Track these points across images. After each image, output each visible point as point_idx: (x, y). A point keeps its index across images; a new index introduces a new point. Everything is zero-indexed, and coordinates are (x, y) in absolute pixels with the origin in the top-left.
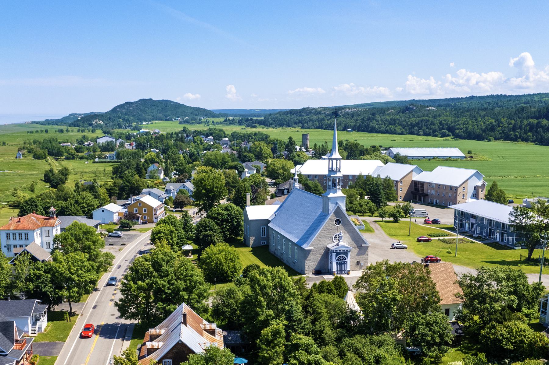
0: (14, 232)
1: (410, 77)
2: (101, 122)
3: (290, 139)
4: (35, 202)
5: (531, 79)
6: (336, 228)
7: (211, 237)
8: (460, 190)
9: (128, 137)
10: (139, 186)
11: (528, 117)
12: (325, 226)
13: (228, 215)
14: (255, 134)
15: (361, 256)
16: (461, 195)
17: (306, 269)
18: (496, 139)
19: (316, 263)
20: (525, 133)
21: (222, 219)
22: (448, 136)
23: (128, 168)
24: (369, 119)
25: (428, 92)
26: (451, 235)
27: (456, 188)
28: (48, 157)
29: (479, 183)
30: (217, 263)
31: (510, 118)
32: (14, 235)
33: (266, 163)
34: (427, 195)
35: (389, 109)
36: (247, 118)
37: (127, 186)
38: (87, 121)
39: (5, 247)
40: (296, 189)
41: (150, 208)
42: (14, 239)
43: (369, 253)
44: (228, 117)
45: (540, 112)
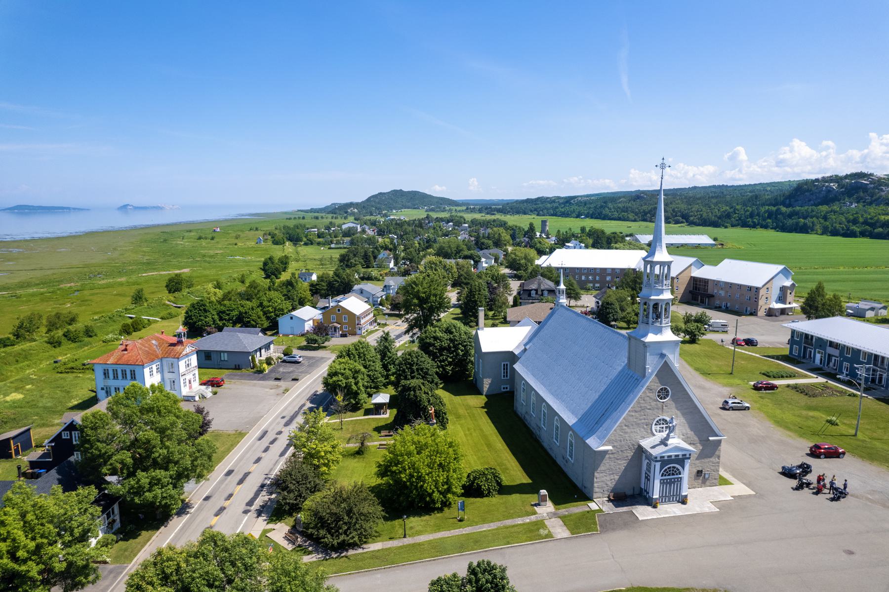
0: (115, 367)
1: (632, 171)
2: (356, 210)
3: (531, 225)
4: (204, 305)
5: (744, 172)
6: (660, 405)
7: (415, 391)
8: (762, 292)
9: (373, 223)
10: (350, 281)
11: (763, 205)
12: (638, 403)
13: (450, 339)
14: (494, 221)
15: (706, 460)
16: (764, 298)
17: (596, 490)
18: (733, 226)
19: (617, 477)
20: (764, 220)
21: (441, 346)
22: (682, 222)
23: (355, 255)
24: (601, 207)
25: (649, 183)
26: (806, 377)
27: (758, 289)
28: (287, 243)
29: (788, 283)
30: (411, 476)
31: (745, 204)
32: (115, 372)
33: (506, 251)
34: (712, 296)
35: (620, 198)
36: (487, 207)
37: (336, 281)
38: (342, 210)
39: (102, 389)
40: (562, 306)
41: (351, 315)
42: (114, 378)
43: (722, 454)
44: (470, 206)
45: (776, 199)
